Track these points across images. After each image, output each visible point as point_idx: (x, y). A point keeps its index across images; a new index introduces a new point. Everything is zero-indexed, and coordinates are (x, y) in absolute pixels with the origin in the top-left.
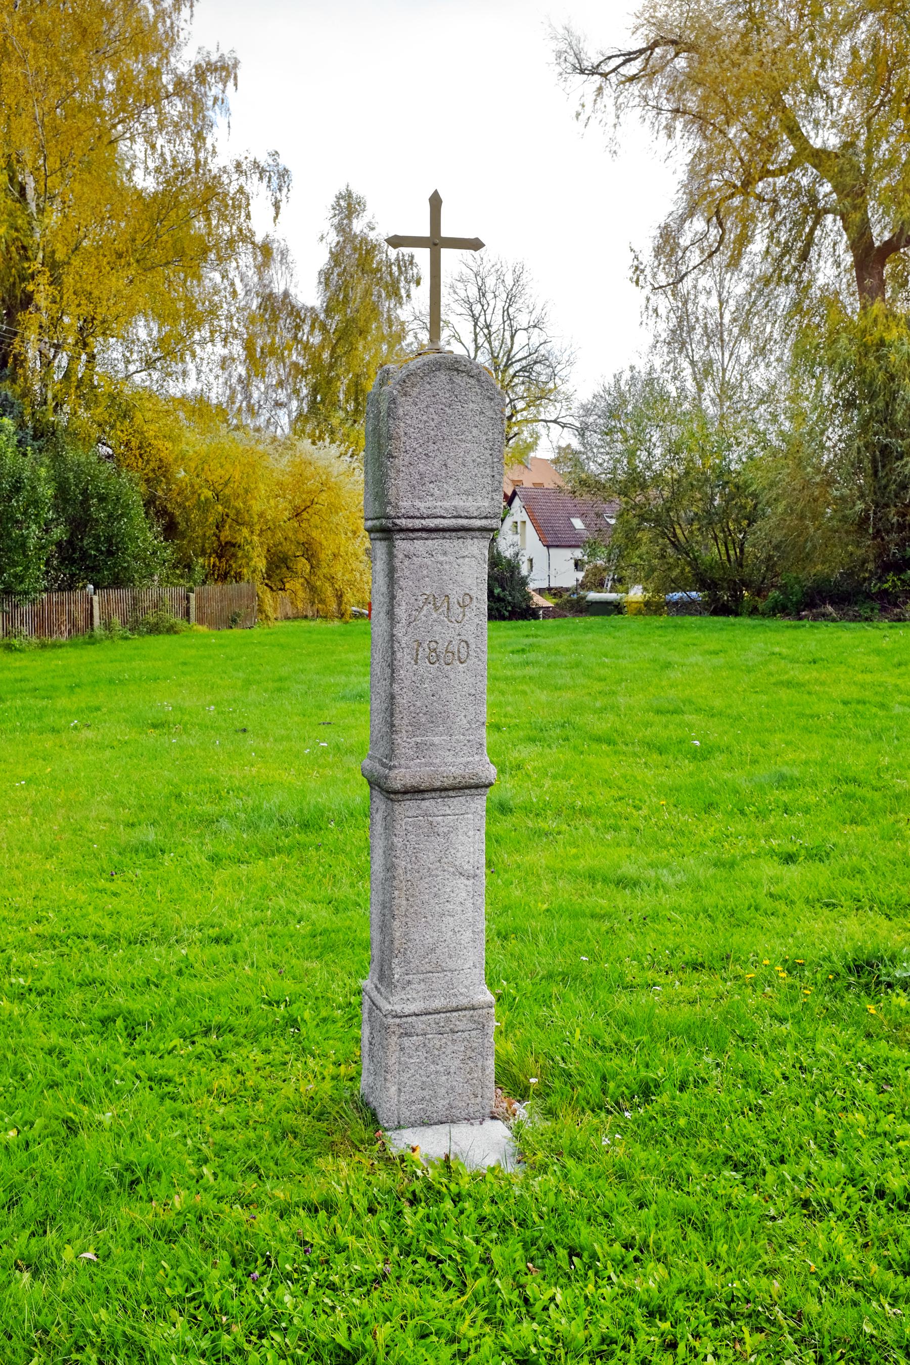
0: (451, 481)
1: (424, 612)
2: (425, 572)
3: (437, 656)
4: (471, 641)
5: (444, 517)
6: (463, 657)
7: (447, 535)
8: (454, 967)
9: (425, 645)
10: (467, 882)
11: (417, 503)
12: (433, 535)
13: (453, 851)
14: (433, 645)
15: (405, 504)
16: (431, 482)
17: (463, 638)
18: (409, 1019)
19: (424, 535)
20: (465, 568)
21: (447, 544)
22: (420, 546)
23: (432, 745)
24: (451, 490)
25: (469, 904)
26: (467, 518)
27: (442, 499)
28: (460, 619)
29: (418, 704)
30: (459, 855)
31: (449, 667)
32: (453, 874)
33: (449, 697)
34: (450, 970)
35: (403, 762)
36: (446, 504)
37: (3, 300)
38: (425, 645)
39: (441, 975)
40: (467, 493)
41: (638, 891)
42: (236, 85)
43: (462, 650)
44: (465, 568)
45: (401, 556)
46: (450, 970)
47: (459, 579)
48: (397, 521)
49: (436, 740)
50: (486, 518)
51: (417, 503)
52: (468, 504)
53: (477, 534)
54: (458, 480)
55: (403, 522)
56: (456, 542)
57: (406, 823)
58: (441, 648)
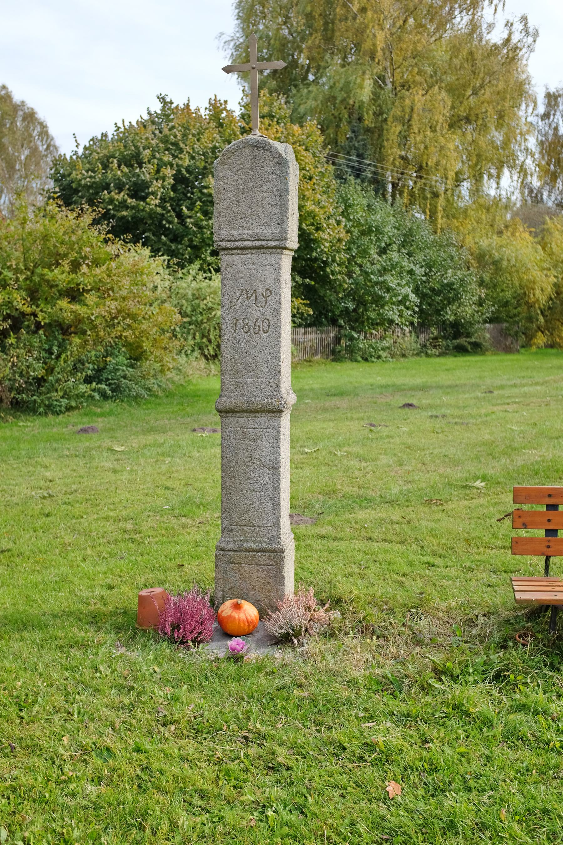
0: (254, 217)
1: (240, 300)
2: (240, 275)
3: (249, 328)
4: (271, 319)
5: (249, 240)
6: (266, 328)
7: (254, 251)
8: (261, 525)
9: (241, 321)
10: (269, 472)
11: (233, 232)
12: (246, 252)
13: (260, 451)
14: (246, 321)
15: (224, 232)
16: (242, 218)
17: (266, 317)
18: (230, 553)
19: (239, 251)
20: (266, 273)
21: (254, 257)
22: (237, 258)
23: (246, 383)
24: (255, 223)
25: (270, 486)
26: (264, 240)
27: (249, 229)
28: (263, 305)
29: (237, 357)
30: (263, 454)
31: (257, 335)
32: (260, 465)
33: (257, 354)
34: (258, 526)
35: (227, 393)
36: (250, 232)
37: (239, 103)
38: (241, 321)
39: (252, 528)
40: (265, 225)
41: (107, 799)
42: (504, 5)
43: (265, 325)
44: (266, 273)
45: (225, 265)
46: (258, 526)
47: (263, 279)
48: (220, 243)
49: (249, 381)
50: (277, 240)
51: (233, 232)
52: (265, 232)
53: (273, 250)
54: (259, 216)
55: (223, 244)
56: (260, 256)
57: (229, 431)
58: (251, 324)
